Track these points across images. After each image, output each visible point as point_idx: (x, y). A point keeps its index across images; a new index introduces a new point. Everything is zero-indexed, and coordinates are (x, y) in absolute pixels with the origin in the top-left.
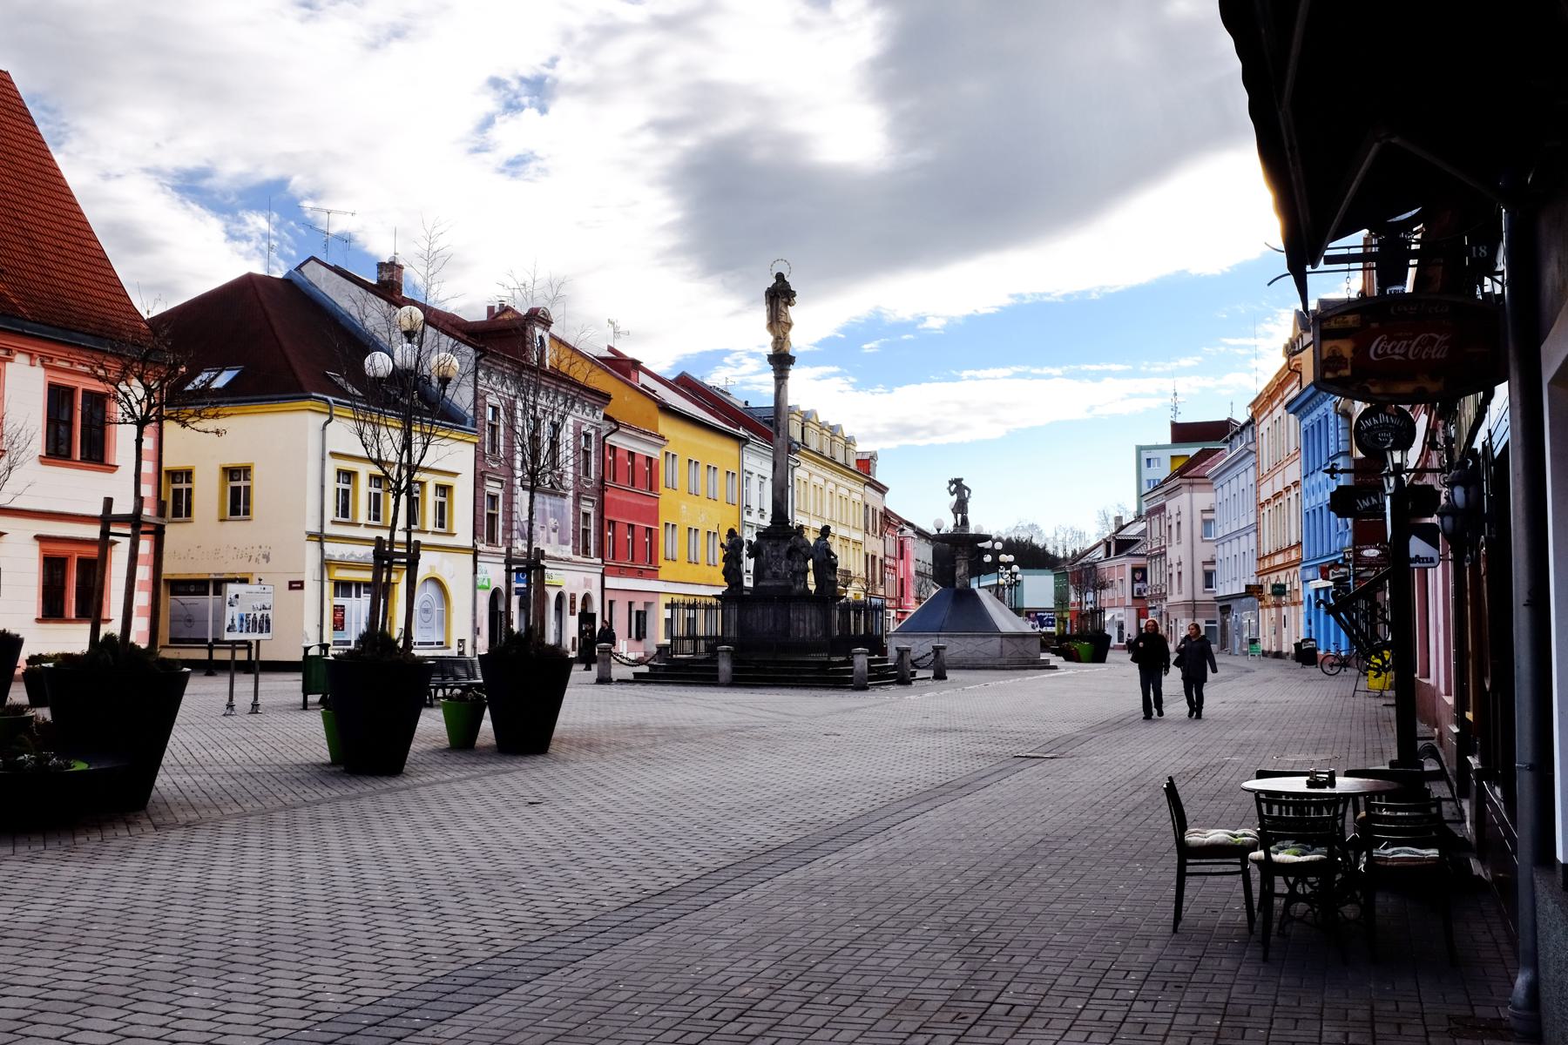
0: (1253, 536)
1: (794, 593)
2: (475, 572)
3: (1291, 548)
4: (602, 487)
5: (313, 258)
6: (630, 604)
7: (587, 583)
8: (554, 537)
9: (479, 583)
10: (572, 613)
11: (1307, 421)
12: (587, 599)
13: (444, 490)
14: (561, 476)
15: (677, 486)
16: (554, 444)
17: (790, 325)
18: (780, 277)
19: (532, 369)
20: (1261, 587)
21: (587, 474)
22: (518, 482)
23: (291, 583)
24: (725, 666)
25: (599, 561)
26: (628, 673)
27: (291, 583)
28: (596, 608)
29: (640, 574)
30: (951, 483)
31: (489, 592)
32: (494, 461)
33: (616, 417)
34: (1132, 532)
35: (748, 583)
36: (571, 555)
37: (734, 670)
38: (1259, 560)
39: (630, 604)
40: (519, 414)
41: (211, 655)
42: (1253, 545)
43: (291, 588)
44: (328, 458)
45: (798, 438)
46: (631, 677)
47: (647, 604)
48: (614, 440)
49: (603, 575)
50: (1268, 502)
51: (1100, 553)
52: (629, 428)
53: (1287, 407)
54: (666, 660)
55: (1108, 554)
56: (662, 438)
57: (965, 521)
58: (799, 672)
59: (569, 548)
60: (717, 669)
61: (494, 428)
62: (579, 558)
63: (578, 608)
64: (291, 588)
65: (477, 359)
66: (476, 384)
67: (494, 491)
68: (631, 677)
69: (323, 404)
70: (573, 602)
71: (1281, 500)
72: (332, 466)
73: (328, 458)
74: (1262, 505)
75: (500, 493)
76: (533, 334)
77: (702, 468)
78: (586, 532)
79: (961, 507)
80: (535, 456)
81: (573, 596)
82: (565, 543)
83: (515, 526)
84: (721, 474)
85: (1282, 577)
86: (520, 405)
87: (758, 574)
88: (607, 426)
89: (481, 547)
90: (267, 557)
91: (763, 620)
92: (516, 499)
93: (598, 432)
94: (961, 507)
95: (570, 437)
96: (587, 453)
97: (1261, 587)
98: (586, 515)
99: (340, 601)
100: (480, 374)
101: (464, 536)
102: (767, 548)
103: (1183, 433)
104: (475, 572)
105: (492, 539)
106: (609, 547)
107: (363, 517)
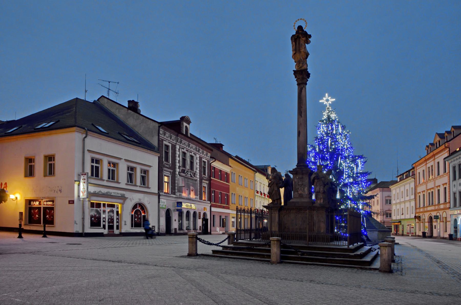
2: (159, 202)
5: (103, 96)
9: (160, 206)
10: (200, 218)
12: (205, 214)
15: (235, 182)
16: (192, 163)
17: (307, 55)
18: (300, 28)
19: (183, 134)
20: (420, 217)
22: (177, 173)
23: (69, 201)
24: (275, 250)
25: (209, 202)
26: (209, 250)
27: (69, 201)
28: (208, 217)
29: (224, 207)
32: (167, 164)
36: (199, 200)
37: (282, 252)
38: (416, 209)
39: (220, 216)
40: (177, 150)
41: (45, 229)
43: (69, 203)
44: (86, 152)
46: (210, 253)
49: (211, 207)
59: (198, 197)
60: (269, 251)
61: (167, 153)
63: (202, 217)
64: (69, 203)
65: (159, 127)
66: (159, 136)
68: (210, 253)
69: (84, 130)
72: (88, 157)
80: (184, 165)
81: (200, 213)
83: (176, 188)
86: (178, 147)
90: (60, 191)
92: (176, 179)
93: (208, 161)
95: (198, 161)
96: (204, 168)
97: (420, 217)
104: (159, 202)
106: (213, 198)
107: (138, 183)
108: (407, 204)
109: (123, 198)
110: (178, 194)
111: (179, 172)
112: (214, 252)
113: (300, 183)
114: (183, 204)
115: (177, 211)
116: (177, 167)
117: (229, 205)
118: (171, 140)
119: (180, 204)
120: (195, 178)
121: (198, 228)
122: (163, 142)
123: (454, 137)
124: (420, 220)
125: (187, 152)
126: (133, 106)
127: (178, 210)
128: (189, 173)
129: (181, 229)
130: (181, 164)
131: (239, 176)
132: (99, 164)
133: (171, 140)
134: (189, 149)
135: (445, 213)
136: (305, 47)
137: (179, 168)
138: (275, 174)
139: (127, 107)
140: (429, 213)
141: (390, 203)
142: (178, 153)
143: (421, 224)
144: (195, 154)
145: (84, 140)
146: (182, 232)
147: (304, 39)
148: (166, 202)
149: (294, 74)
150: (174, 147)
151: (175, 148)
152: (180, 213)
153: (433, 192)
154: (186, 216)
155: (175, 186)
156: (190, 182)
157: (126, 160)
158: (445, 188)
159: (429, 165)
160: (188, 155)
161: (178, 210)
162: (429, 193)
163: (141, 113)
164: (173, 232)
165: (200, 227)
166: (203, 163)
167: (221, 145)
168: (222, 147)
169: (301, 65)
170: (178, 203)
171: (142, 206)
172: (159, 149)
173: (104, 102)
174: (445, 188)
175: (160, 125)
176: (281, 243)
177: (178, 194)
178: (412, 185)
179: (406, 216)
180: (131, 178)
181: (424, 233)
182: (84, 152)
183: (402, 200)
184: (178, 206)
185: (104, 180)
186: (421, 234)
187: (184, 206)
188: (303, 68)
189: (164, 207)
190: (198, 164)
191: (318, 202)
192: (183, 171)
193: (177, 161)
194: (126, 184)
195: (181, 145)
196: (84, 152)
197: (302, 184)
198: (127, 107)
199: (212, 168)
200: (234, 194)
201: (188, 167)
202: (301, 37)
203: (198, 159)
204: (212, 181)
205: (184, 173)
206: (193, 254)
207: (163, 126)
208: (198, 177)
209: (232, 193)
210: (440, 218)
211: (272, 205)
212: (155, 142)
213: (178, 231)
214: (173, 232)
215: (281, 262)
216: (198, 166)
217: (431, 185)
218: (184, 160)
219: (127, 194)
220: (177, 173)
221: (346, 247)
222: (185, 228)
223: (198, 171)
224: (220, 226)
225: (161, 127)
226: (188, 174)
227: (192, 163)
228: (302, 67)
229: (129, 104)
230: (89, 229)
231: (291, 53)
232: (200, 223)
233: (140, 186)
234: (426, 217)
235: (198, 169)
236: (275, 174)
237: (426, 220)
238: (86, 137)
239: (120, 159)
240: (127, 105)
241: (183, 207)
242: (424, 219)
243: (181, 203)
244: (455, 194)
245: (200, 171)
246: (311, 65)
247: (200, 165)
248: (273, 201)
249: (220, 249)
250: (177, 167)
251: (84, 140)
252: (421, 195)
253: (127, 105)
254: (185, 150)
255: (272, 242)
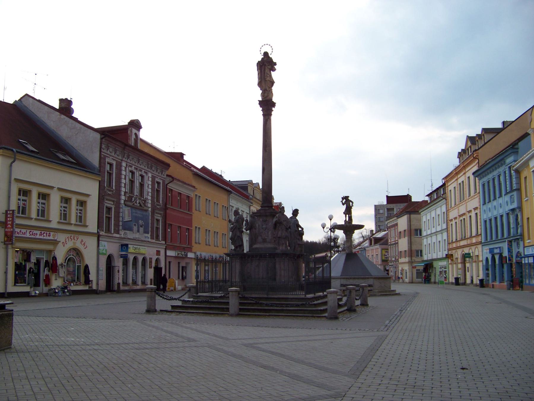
0: (445, 235)
1: (278, 251)
2: (98, 246)
3: (471, 237)
4: (165, 209)
6: (179, 263)
7: (158, 253)
8: (141, 229)
9: (101, 251)
10: (151, 267)
11: (485, 179)
12: (157, 260)
13: (82, 204)
14: (145, 201)
16: (142, 185)
17: (272, 83)
18: (266, 54)
19: (130, 146)
20: (452, 255)
21: (158, 201)
22: (122, 202)
24: (234, 302)
25: (164, 242)
28: (162, 265)
30: (343, 198)
31: (106, 257)
32: (110, 191)
33: (173, 176)
34: (380, 235)
35: (246, 249)
37: (241, 304)
38: (449, 244)
39: (179, 263)
40: (123, 168)
42: (445, 237)
44: (13, 183)
45: (252, 194)
46: (170, 309)
47: (187, 263)
48: (171, 186)
49: (166, 249)
50: (455, 218)
51: (367, 244)
52: (179, 180)
53: (473, 174)
54: (193, 297)
55: (371, 244)
56: (194, 187)
57: (350, 218)
58: (287, 305)
59: (149, 235)
60: (228, 303)
61: (110, 174)
62: (154, 241)
63: (153, 265)
65: (101, 139)
66: (100, 151)
67: (159, 218)
68: (170, 309)
70: (151, 262)
71: (464, 217)
73: (13, 183)
74: (451, 220)
75: (113, 207)
76: (131, 131)
77: (212, 204)
78: (158, 228)
79: (348, 211)
81: (151, 259)
82: (148, 233)
83: (121, 223)
84: (220, 207)
85: (466, 250)
86: (124, 164)
87: (252, 242)
88: (168, 179)
89: (102, 233)
91: (258, 270)
92: (121, 210)
93: (164, 182)
94: (348, 211)
95: (150, 183)
96: (158, 191)
97: (452, 255)
98: (158, 220)
99: (487, 278)
100: (103, 146)
101: (92, 225)
102: (259, 223)
103: (391, 200)
104: (98, 246)
105: (108, 230)
106: (169, 236)
108: (439, 237)
109: (55, 243)
110: (122, 232)
111: (125, 201)
112: (173, 307)
113: (264, 226)
114: (129, 246)
115: (121, 257)
116: (123, 193)
117: (192, 211)
118: (116, 156)
119: (124, 247)
120: (145, 208)
121: (149, 282)
122: (105, 159)
123: (485, 144)
124: (452, 260)
125: (135, 171)
126: (66, 106)
127: (121, 256)
128: (138, 202)
129: (125, 283)
130: (128, 187)
131: (207, 199)
132: (27, 196)
133: (116, 156)
134: (139, 165)
135: (477, 249)
136: (271, 76)
137: (125, 195)
138: (238, 216)
139: (57, 107)
140: (461, 250)
141: (420, 235)
142: (123, 173)
143: (454, 265)
144: (146, 173)
145: (11, 166)
146: (126, 288)
147: (269, 67)
148: (110, 247)
149: (259, 104)
150: (119, 166)
151: (121, 166)
152: (125, 259)
153: (464, 219)
154: (133, 265)
155: (119, 221)
156: (139, 213)
157: (60, 189)
158: (476, 214)
159: (460, 181)
160: (137, 174)
161: (121, 256)
162: (461, 220)
163: (74, 115)
164: (116, 288)
165: (151, 280)
166: (156, 185)
167: (182, 155)
168: (183, 157)
169: (266, 94)
170: (122, 245)
171: (77, 252)
172: (100, 171)
173: (26, 102)
174: (476, 214)
175: (103, 136)
176: (239, 294)
177: (122, 232)
178: (444, 209)
179: (439, 253)
180: (64, 216)
181: (457, 279)
182: (10, 182)
183: (434, 231)
184: (122, 251)
185: (32, 219)
186: (454, 281)
187: (131, 249)
188: (268, 98)
189: (104, 252)
190: (150, 187)
191: (281, 248)
192: (130, 199)
193: (123, 185)
194: (59, 222)
195: (129, 161)
196: (10, 182)
197: (266, 228)
198: (57, 107)
199: (168, 191)
200: (199, 228)
201: (136, 192)
202: (266, 65)
203: (150, 179)
204: (168, 211)
205: (131, 201)
206: (151, 310)
207: (107, 138)
208: (149, 205)
209: (196, 227)
210: (472, 256)
211: (234, 252)
212: (94, 159)
213: (122, 288)
214: (116, 288)
215: (238, 315)
216: (150, 190)
217: (462, 210)
218: (132, 182)
219: (61, 237)
220: (122, 202)
221: (303, 296)
222: (130, 281)
223: (150, 198)
224: (179, 278)
225: (104, 140)
226: (136, 202)
227: (142, 185)
228: (267, 97)
229: (60, 103)
230: (11, 289)
231: (256, 80)
232: (150, 273)
233: (75, 225)
234: (458, 254)
235: (150, 194)
236: (238, 216)
237: (459, 261)
238: (14, 162)
239: (52, 188)
240: (57, 106)
241: (130, 251)
242: (457, 258)
243: (127, 245)
244: (485, 221)
245: (152, 197)
246: (278, 94)
247: (153, 185)
248: (236, 247)
249: (179, 303)
250: (123, 193)
251: (11, 166)
252: (453, 223)
253: (57, 106)
254: (133, 169)
255: (230, 293)
